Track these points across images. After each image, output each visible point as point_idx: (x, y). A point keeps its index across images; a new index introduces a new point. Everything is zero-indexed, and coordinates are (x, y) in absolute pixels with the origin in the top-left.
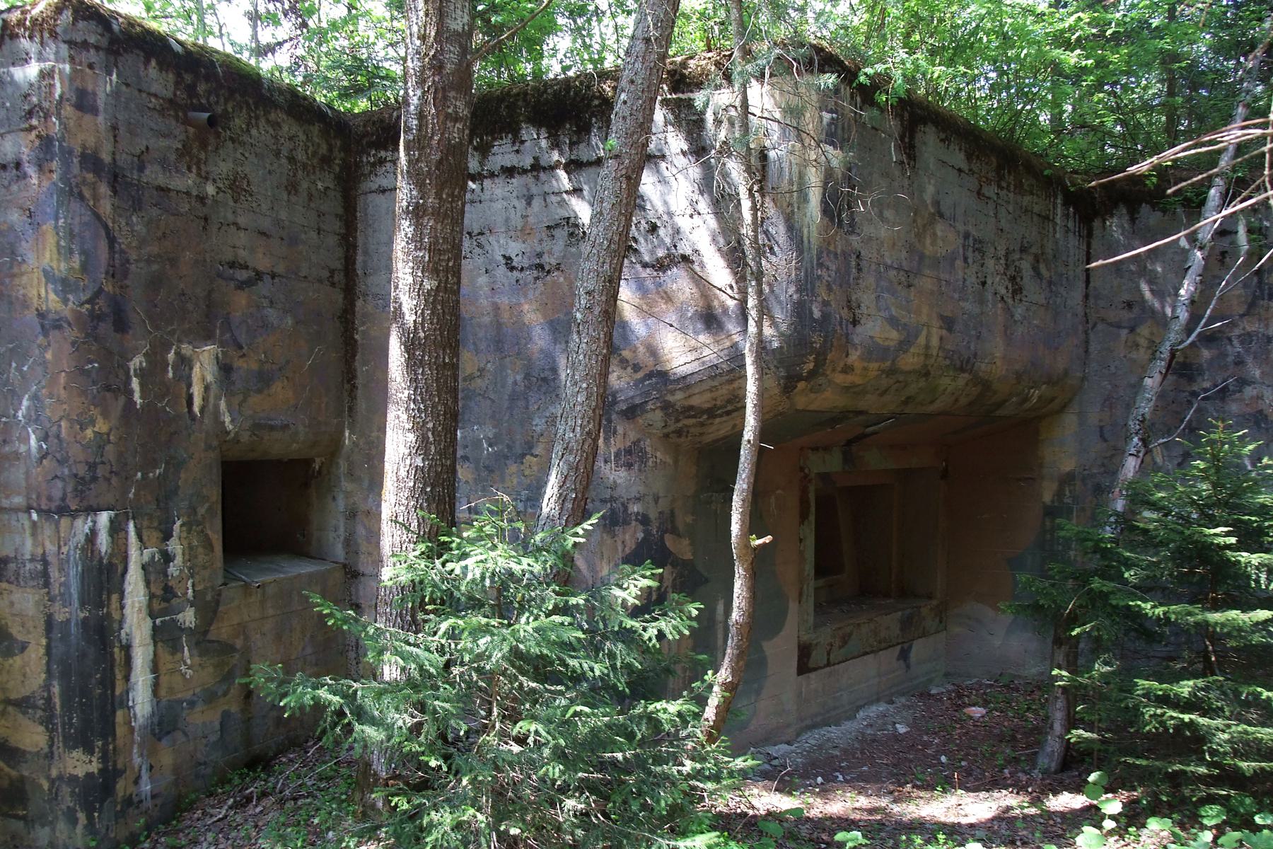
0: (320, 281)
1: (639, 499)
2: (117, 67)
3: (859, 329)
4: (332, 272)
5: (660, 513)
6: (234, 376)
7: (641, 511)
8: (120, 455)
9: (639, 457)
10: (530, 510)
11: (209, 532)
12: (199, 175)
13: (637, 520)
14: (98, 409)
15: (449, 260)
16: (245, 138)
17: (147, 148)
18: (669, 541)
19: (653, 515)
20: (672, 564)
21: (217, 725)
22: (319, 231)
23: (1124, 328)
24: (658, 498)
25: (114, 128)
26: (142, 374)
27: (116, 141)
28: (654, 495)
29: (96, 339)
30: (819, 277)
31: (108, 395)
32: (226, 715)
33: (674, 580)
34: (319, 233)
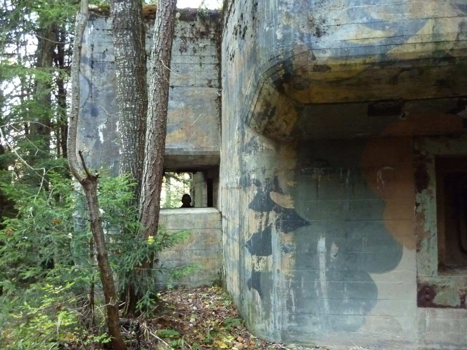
0: (202, 86)
1: (254, 171)
2: (93, 24)
3: (323, 38)
4: (210, 81)
5: (266, 179)
7: (256, 178)
8: (93, 160)
9: (254, 147)
13: (254, 183)
14: (84, 144)
15: (125, 63)
17: (107, 50)
18: (273, 196)
19: (262, 180)
20: (274, 210)
22: (201, 64)
24: (265, 170)
25: (92, 46)
26: (104, 131)
27: (92, 49)
28: (262, 168)
29: (84, 119)
30: (280, 12)
31: (88, 139)
33: (278, 220)
34: (201, 66)
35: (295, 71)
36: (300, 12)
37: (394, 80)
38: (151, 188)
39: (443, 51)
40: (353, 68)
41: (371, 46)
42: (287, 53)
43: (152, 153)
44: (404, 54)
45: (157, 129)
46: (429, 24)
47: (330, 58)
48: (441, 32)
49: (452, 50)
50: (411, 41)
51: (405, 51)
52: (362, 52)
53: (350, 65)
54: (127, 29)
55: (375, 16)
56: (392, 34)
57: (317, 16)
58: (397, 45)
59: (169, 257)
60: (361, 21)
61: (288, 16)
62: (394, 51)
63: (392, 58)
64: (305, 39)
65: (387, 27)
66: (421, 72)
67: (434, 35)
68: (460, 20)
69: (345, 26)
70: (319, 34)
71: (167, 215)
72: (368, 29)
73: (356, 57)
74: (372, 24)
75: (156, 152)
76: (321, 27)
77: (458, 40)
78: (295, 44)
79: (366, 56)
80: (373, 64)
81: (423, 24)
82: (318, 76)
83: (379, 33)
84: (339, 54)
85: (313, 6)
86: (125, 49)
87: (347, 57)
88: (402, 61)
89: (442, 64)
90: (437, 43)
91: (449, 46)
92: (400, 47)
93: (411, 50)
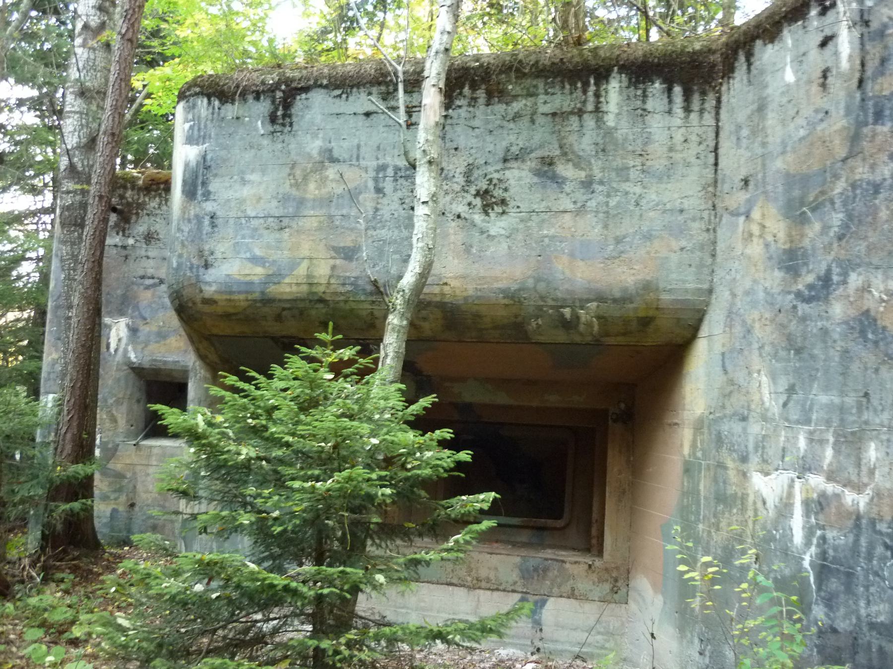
3: (211, 271)
6: (139, 334)
10: (736, 447)
11: (114, 412)
12: (124, 235)
15: (70, 264)
16: (158, 212)
21: (108, 514)
23: (742, 214)
30: (178, 238)
32: (114, 511)
35: (187, 302)
36: (193, 241)
37: (279, 318)
38: (68, 413)
39: (315, 293)
40: (238, 304)
41: (251, 283)
42: (178, 283)
43: (71, 375)
44: (282, 293)
45: (78, 348)
46: (305, 264)
47: (215, 291)
48: (315, 274)
49: (324, 293)
50: (287, 280)
51: (282, 290)
52: (243, 288)
53: (234, 300)
54: (75, 225)
55: (258, 252)
56: (271, 272)
57: (207, 247)
58: (275, 283)
59: (149, 502)
60: (244, 256)
61: (183, 245)
62: (273, 290)
63: (271, 296)
64: (194, 270)
65: (267, 265)
66: (301, 312)
67: (309, 276)
68: (332, 262)
69: (230, 260)
70: (207, 266)
71: (151, 447)
72: (250, 265)
73: (239, 293)
74: (255, 260)
75: (75, 374)
76: (210, 259)
77: (329, 284)
78: (185, 275)
79: (247, 292)
80: (255, 301)
81: (299, 264)
82: (207, 309)
83: (259, 270)
84: (223, 289)
85: (204, 237)
86: (72, 248)
87: (231, 293)
88: (280, 301)
89: (318, 306)
90: (311, 284)
91: (322, 289)
92: (277, 286)
93: (288, 290)
